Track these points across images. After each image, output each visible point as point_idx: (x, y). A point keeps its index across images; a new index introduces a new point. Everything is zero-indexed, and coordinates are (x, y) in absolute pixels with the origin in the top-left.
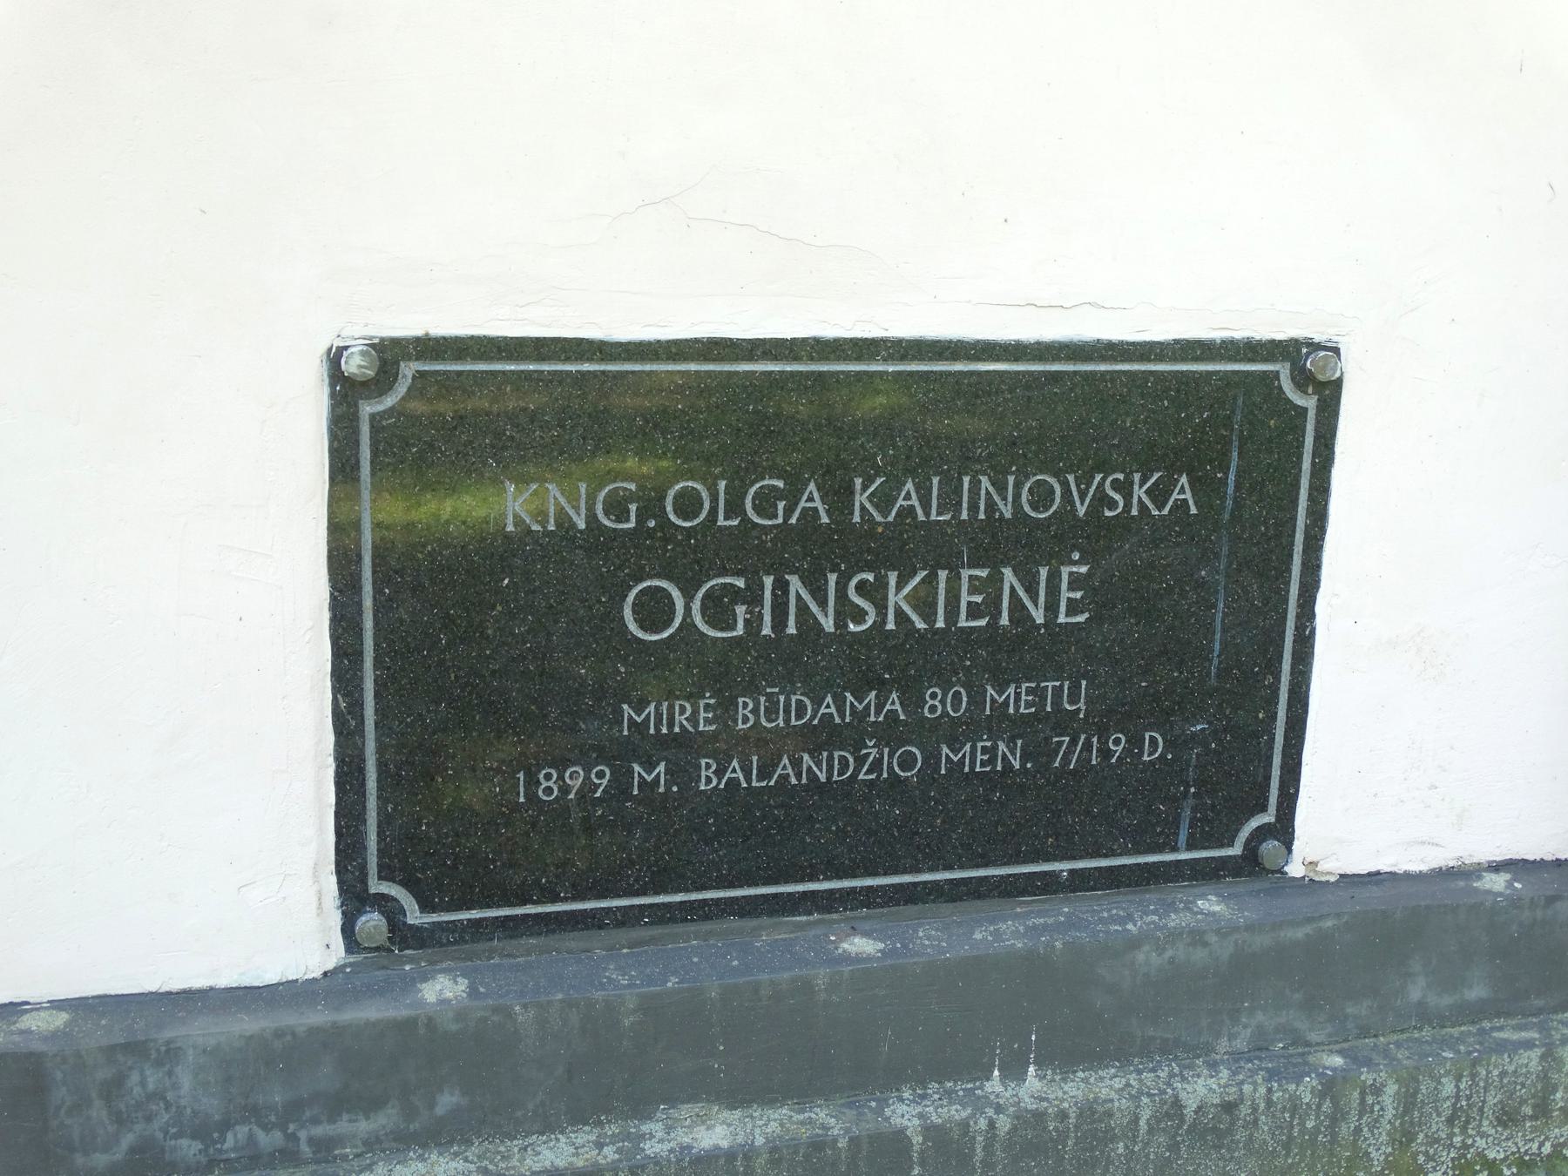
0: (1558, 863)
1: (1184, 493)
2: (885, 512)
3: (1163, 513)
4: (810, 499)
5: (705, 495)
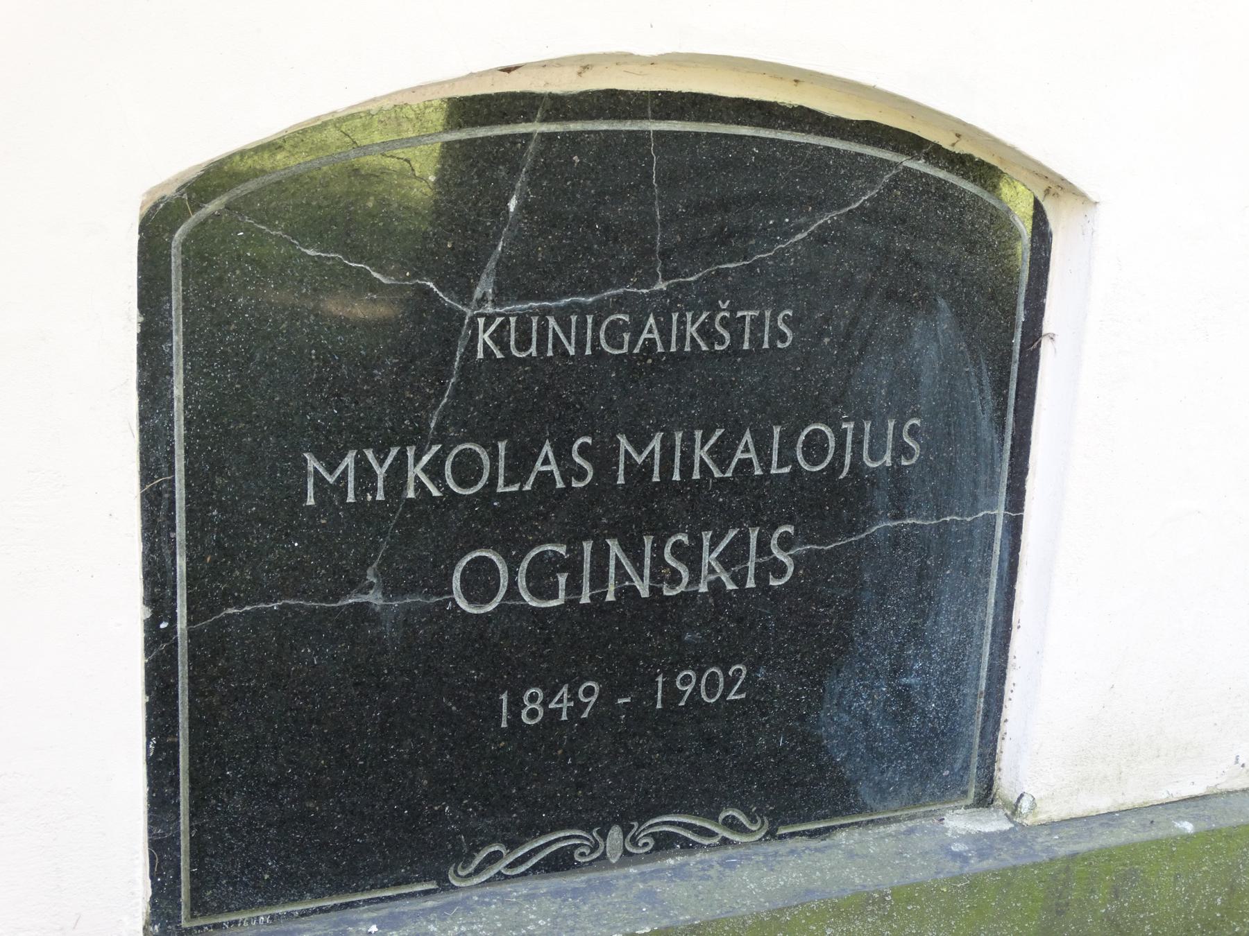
0: (1244, 791)
1: (549, 463)
2: (723, 466)
3: (726, 475)
4: (747, 450)
5: (486, 462)
